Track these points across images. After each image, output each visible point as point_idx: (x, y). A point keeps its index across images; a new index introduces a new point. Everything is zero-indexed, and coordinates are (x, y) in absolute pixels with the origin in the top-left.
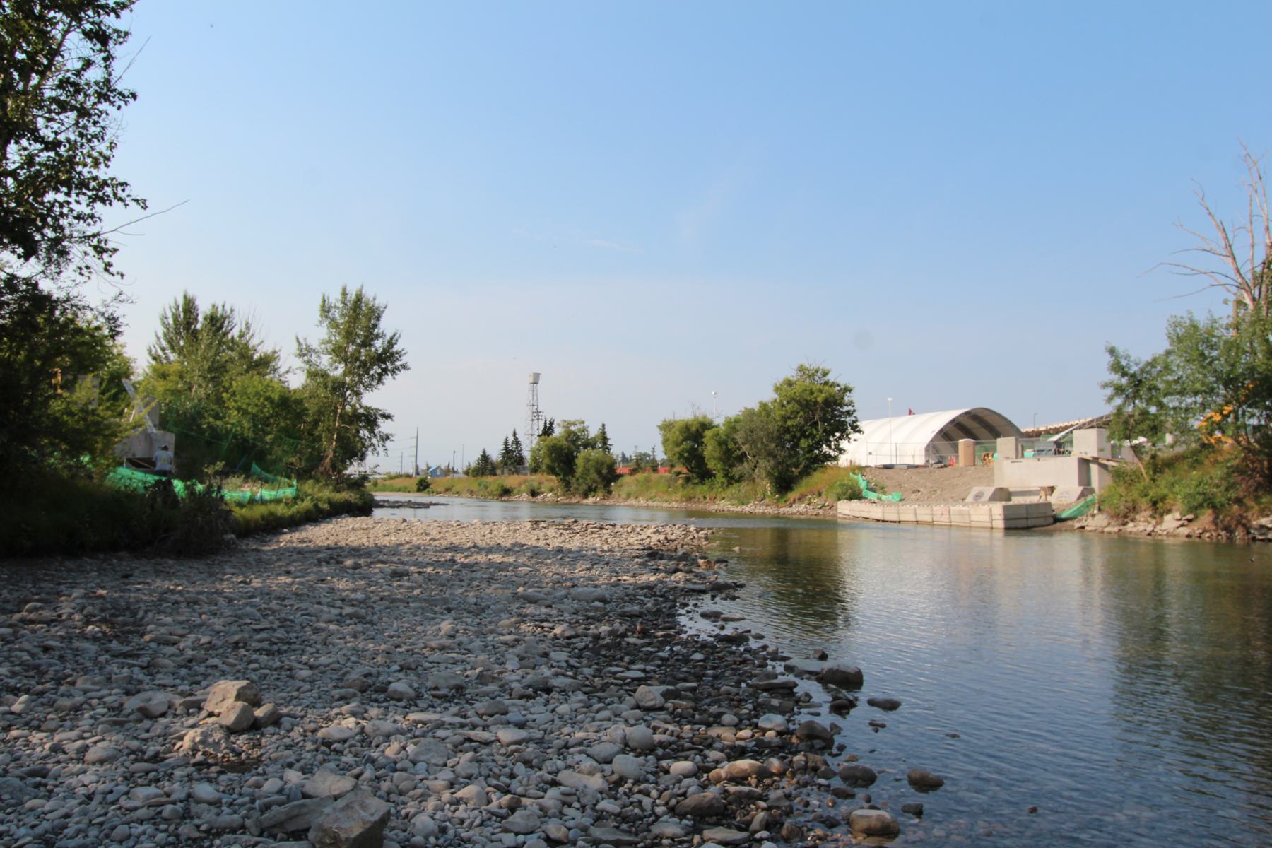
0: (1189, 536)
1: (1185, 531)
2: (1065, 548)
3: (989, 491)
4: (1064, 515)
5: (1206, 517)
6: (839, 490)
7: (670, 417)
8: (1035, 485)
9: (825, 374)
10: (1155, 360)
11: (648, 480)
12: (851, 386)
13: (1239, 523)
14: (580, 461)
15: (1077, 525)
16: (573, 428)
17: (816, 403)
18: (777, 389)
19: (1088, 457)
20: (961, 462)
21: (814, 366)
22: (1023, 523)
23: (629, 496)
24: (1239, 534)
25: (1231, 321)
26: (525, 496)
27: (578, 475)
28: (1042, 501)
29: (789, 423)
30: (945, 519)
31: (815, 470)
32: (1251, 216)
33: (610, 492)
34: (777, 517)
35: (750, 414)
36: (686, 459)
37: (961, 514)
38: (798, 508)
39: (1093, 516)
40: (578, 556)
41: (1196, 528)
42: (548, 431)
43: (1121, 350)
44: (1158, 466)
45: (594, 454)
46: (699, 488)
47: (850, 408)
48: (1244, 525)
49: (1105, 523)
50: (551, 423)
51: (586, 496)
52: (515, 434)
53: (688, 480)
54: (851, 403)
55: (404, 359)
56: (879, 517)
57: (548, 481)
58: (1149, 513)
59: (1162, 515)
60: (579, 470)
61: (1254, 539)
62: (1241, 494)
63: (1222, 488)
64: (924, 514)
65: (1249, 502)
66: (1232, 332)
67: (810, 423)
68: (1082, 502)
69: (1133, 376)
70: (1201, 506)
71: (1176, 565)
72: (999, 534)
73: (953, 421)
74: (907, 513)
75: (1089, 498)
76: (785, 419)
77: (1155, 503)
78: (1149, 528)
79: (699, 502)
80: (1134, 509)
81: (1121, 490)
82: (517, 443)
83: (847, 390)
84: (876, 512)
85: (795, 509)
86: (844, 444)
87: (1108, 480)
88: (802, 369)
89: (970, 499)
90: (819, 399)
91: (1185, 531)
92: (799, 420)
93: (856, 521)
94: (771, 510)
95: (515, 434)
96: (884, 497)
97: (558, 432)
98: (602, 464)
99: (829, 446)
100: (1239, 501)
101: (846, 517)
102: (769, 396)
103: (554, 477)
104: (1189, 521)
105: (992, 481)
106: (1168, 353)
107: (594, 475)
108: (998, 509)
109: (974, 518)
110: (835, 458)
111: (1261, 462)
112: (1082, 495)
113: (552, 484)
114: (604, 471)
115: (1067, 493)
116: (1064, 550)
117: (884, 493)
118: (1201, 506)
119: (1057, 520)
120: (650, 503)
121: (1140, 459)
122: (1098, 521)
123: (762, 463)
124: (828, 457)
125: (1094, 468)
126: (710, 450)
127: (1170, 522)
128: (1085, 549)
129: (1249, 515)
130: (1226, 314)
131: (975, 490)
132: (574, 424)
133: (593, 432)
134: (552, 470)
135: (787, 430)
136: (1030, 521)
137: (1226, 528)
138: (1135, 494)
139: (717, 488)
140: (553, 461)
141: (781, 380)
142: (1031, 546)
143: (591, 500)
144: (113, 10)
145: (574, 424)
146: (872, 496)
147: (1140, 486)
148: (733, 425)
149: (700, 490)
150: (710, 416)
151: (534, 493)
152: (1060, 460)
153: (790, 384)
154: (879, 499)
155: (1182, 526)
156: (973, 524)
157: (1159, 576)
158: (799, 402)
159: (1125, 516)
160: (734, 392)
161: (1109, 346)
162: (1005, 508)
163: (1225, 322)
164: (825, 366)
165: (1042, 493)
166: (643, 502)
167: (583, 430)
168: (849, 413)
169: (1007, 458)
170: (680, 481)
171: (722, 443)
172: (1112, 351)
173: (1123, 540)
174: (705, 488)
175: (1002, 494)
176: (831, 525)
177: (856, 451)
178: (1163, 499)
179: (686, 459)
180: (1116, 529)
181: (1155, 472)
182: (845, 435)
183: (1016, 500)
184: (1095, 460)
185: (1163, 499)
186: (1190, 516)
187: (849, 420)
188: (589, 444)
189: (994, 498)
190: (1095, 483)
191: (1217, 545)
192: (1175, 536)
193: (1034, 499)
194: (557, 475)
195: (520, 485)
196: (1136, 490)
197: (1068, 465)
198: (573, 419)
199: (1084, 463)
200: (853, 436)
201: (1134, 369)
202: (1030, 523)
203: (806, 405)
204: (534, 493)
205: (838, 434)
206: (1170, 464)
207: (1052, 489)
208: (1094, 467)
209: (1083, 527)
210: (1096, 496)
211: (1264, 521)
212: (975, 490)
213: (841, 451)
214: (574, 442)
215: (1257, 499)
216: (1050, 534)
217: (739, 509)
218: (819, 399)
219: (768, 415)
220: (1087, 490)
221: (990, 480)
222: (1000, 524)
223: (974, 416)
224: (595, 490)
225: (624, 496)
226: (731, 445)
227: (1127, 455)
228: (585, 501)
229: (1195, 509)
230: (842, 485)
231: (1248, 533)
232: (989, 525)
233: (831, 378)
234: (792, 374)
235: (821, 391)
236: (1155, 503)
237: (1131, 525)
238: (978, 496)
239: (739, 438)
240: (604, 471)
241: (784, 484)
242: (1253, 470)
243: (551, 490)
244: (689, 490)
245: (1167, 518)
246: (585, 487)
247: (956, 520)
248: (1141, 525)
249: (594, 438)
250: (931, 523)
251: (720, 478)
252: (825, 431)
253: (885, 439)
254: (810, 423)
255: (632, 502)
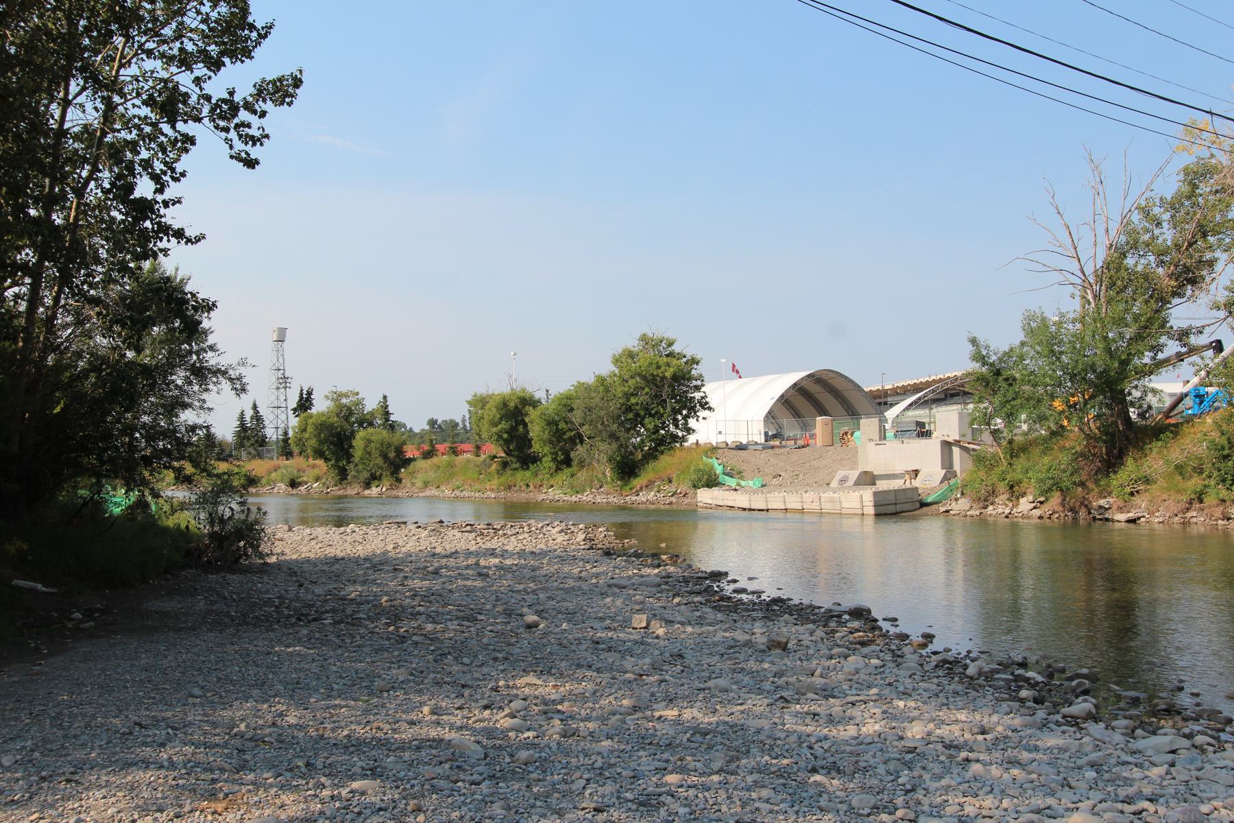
0: (1040, 517)
1: (1037, 512)
2: (930, 531)
3: (854, 475)
4: (929, 500)
5: (1056, 499)
6: (694, 477)
7: (482, 391)
8: (899, 468)
9: (670, 344)
10: (1011, 350)
11: (451, 465)
12: (698, 357)
13: (1082, 503)
14: (358, 442)
15: (942, 509)
16: (344, 401)
17: (663, 378)
18: (616, 361)
19: (950, 440)
20: (819, 441)
21: (658, 335)
22: (892, 509)
23: (426, 484)
24: (1082, 513)
25: (1077, 315)
26: (282, 486)
27: (356, 459)
28: (908, 485)
29: (633, 400)
30: (815, 506)
31: (662, 453)
32: (1095, 215)
33: (399, 480)
34: (623, 508)
35: (582, 386)
36: (506, 441)
37: (832, 501)
38: (646, 495)
39: (957, 500)
40: (492, 553)
41: (1045, 510)
42: (305, 403)
43: (981, 340)
44: (1015, 451)
45: (378, 434)
46: (520, 475)
47: (699, 383)
48: (1086, 506)
49: (968, 506)
50: (310, 393)
51: (367, 485)
52: (255, 407)
53: (505, 465)
54: (700, 377)
55: (211, 340)
56: (746, 505)
57: (315, 470)
58: (1006, 496)
59: (1018, 499)
60: (358, 453)
61: (1094, 518)
62: (1084, 478)
63: (1068, 473)
64: (793, 502)
65: (1091, 485)
66: (1078, 326)
67: (656, 397)
68: (945, 486)
69: (992, 365)
70: (1050, 489)
71: (1030, 544)
72: (870, 521)
73: (795, 384)
74: (775, 500)
75: (953, 481)
76: (628, 396)
77: (1012, 487)
78: (1007, 511)
79: (520, 490)
80: (993, 493)
81: (982, 474)
82: (257, 417)
83: (694, 361)
84: (741, 500)
85: (642, 497)
86: (692, 423)
87: (969, 464)
88: (644, 338)
89: (834, 484)
90: (668, 374)
91: (1037, 512)
92: (642, 398)
93: (719, 512)
94: (614, 499)
95: (255, 407)
96: (743, 483)
97: (321, 406)
98: (389, 445)
99: (677, 426)
100: (1082, 484)
101: (708, 507)
102: (606, 368)
103: (320, 462)
104: (1041, 503)
105: (856, 463)
106: (1023, 344)
107: (380, 461)
108: (868, 495)
109: (845, 505)
110: (684, 439)
111: (1101, 448)
112: (945, 479)
113: (316, 471)
114: (392, 455)
115: (931, 477)
116: (929, 533)
117: (742, 478)
118: (1050, 489)
119: (923, 505)
120: (457, 493)
121: (999, 445)
122: (961, 505)
123: (604, 447)
124: (674, 438)
125: (956, 450)
126: (536, 430)
127: (1025, 504)
128: (949, 532)
129: (1090, 496)
130: (1073, 307)
131: (840, 474)
132: (346, 396)
133: (371, 405)
134: (319, 454)
135: (629, 409)
136: (898, 507)
137: (1072, 510)
138: (994, 478)
139: (544, 474)
140: (321, 442)
141: (620, 351)
142: (897, 531)
143: (374, 491)
144: (259, 140)
145: (346, 396)
146: (732, 482)
147: (998, 470)
148: (566, 404)
149: (522, 476)
150: (530, 389)
151: (293, 484)
152: (923, 442)
153: (631, 355)
154: (739, 484)
155: (1035, 508)
156: (844, 511)
157: (1015, 554)
158: (644, 378)
159: (986, 500)
160: (564, 362)
161: (971, 336)
162: (875, 494)
163: (1071, 316)
164: (669, 335)
165: (907, 477)
166: (448, 492)
167: (359, 403)
168: (697, 388)
169: (871, 440)
170: (494, 466)
171: (551, 423)
172: (974, 341)
173: (982, 521)
174: (528, 474)
175: (868, 479)
176: (692, 514)
177: (703, 431)
178: (1019, 482)
179: (506, 441)
180: (978, 513)
181: (1012, 457)
182: (692, 411)
183: (882, 485)
184: (957, 443)
185: (1019, 482)
186: (1042, 499)
187: (697, 395)
188: (366, 422)
189: (858, 483)
190: (957, 467)
191: (1064, 525)
192: (1029, 518)
193: (897, 484)
194: (326, 460)
195: (269, 473)
196: (995, 471)
197: (931, 447)
198: (344, 390)
199: (947, 445)
200: (702, 413)
201: (994, 358)
202: (899, 508)
203: (652, 381)
204: (293, 484)
205: (685, 412)
206: (1024, 449)
207: (916, 472)
208: (956, 450)
209: (947, 511)
210: (958, 481)
211: (1102, 502)
212: (840, 474)
213: (689, 431)
214: (347, 418)
215: (1097, 482)
216: (915, 518)
217: (574, 498)
218: (668, 374)
219: (607, 391)
220: (949, 474)
221: (854, 464)
222: (870, 510)
223: (818, 379)
224: (379, 478)
225: (419, 484)
226: (562, 425)
227: (987, 437)
228: (367, 492)
229: (1047, 492)
230: (698, 471)
231: (1090, 513)
232: (860, 512)
233: (676, 348)
234: (633, 343)
235: (668, 365)
236: (1012, 487)
237: (991, 508)
238: (843, 481)
239: (577, 417)
240: (392, 455)
241: (627, 469)
242: (1094, 455)
243: (317, 479)
244: (508, 476)
245: (1022, 500)
246: (366, 475)
247: (827, 507)
248: (999, 508)
249: (372, 413)
250: (802, 511)
251: (547, 462)
252: (673, 409)
253: (733, 410)
254: (656, 397)
255: (431, 491)
